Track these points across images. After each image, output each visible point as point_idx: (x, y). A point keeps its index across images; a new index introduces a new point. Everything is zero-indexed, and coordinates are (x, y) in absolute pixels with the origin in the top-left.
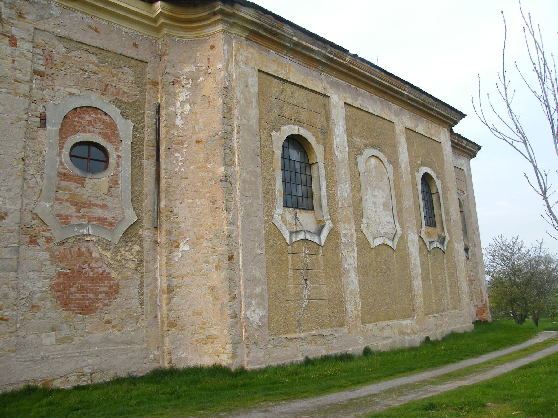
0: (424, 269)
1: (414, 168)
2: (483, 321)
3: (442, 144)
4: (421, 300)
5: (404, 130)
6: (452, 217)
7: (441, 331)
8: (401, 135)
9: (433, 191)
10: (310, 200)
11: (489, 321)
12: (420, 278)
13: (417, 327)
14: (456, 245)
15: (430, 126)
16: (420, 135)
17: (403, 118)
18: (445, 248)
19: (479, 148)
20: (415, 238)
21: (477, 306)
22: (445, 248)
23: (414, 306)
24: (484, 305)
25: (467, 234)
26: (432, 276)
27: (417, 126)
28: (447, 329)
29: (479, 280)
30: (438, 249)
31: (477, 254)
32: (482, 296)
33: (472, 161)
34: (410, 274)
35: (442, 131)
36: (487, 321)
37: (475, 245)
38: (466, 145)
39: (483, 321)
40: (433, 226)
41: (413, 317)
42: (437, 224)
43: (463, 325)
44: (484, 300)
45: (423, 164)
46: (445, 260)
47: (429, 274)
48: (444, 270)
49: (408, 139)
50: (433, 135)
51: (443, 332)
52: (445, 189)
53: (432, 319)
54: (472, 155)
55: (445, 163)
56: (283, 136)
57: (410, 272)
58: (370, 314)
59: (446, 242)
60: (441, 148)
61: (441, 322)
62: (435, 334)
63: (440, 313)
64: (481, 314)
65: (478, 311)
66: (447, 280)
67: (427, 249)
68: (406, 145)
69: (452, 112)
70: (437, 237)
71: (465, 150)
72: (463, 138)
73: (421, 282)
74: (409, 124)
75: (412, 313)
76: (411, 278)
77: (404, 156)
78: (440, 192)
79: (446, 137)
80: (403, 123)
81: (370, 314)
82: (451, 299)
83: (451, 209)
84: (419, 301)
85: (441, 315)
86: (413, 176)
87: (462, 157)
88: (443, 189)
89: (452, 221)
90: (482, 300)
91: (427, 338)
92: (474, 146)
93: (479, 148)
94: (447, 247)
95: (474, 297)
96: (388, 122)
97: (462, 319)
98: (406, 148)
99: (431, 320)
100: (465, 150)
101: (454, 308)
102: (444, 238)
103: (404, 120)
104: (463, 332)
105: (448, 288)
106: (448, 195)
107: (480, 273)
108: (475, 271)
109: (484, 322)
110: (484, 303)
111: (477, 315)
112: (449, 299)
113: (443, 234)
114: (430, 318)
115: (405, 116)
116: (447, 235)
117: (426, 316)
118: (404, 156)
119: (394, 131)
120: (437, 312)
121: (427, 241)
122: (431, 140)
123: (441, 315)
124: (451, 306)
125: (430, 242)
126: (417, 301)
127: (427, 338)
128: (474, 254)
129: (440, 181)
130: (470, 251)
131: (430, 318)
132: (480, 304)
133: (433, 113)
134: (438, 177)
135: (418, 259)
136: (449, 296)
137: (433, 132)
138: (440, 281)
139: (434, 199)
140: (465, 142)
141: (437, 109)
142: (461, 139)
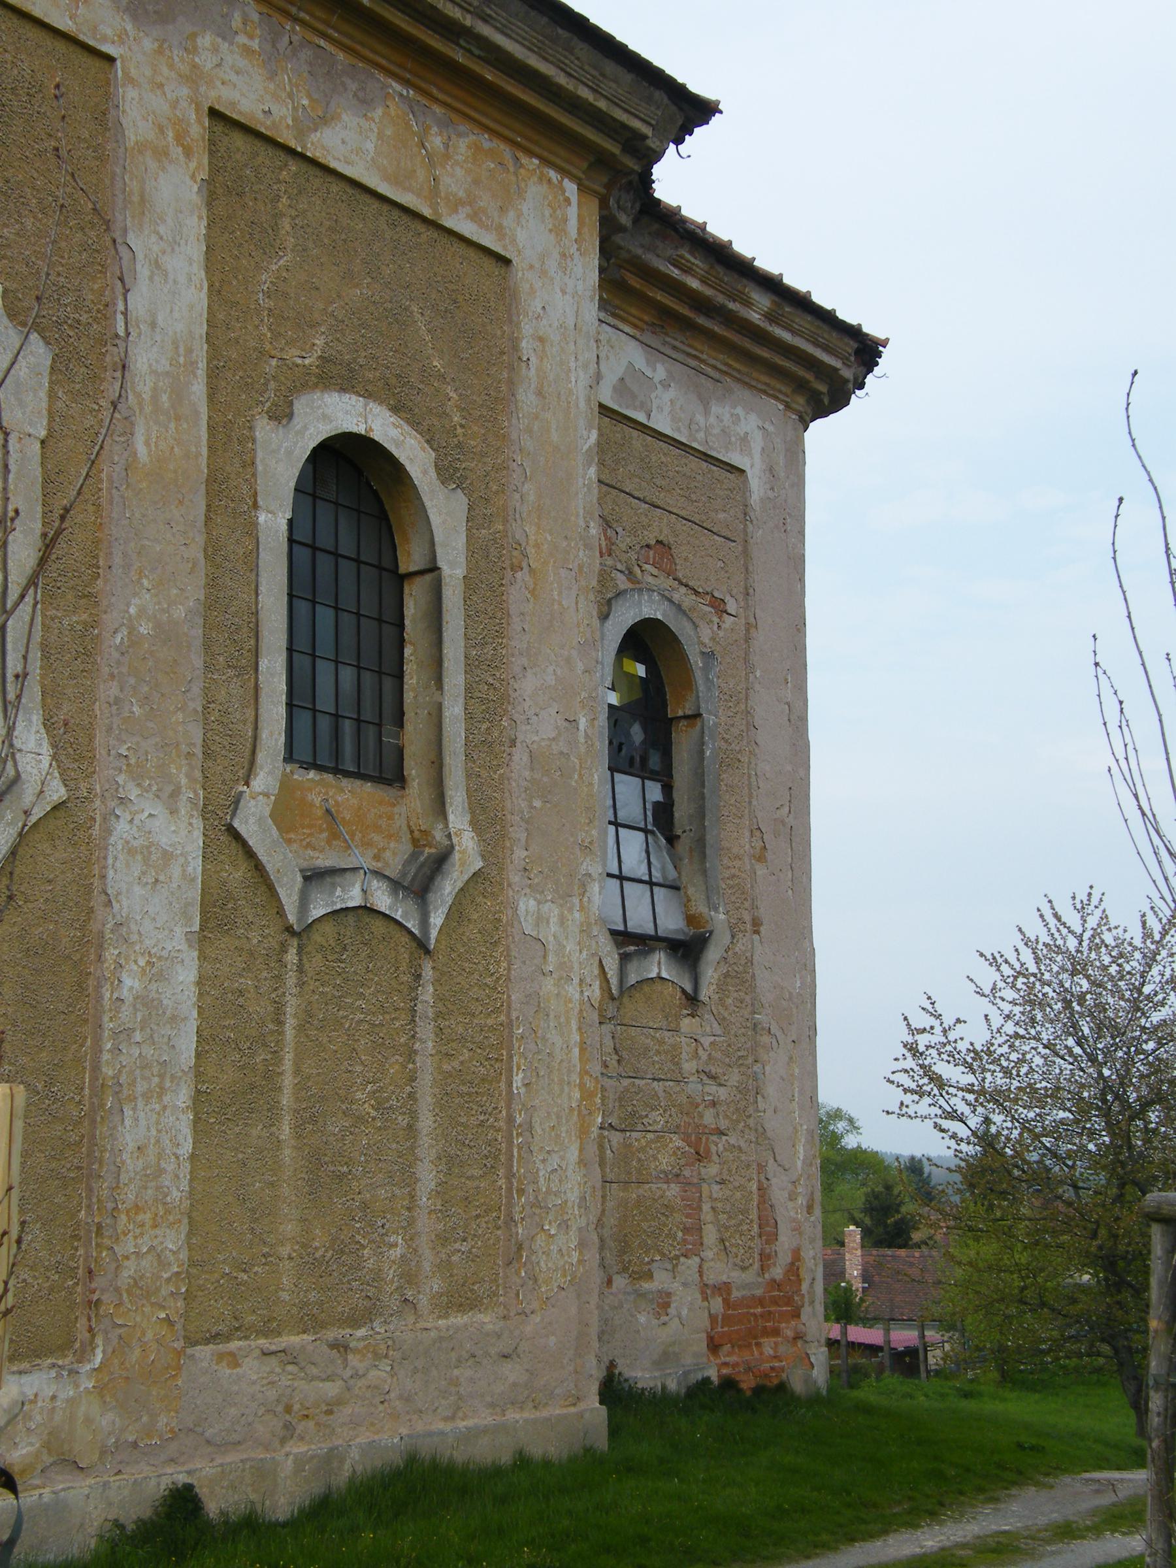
0: (233, 1041)
1: (241, 382)
2: (747, 1383)
3: (521, 271)
4: (173, 1241)
5: (198, 128)
6: (525, 735)
7: (319, 1447)
8: (161, 154)
9: (411, 559)
10: (388, 683)
11: (798, 1386)
12: (183, 1096)
13: (107, 1420)
14: (527, 905)
15: (436, 141)
16: (336, 187)
17: (206, 40)
18: (437, 920)
19: (867, 351)
20: (182, 835)
21: (723, 1289)
22: (437, 920)
23: (99, 1282)
24: (774, 1284)
25: (703, 856)
26: (299, 1087)
27: (324, 120)
28: (369, 1439)
29: (762, 1133)
30: (378, 926)
31: (764, 982)
32: (768, 1229)
33: (822, 435)
34: (96, 1068)
35: (535, 191)
36: (782, 1387)
37: (756, 924)
38: (770, 317)
39: (747, 1383)
40: (380, 779)
41: (83, 1355)
42: (414, 770)
43: (513, 1415)
44: (784, 1259)
45: (336, 375)
46: (427, 994)
47: (271, 1075)
48: (411, 1054)
49: (221, 191)
50: (455, 205)
51: (332, 1457)
52: (494, 561)
53: (251, 1368)
54: (830, 395)
55: (526, 398)
56: (714, 449)
57: (98, 1049)
58: (219, 1312)
59: (448, 887)
60: (507, 300)
61: (332, 1389)
62: (263, 1472)
63: (332, 1334)
64: (749, 1338)
65: (727, 1319)
66: (426, 1122)
67: (281, 912)
68: (195, 226)
69: (610, 67)
70: (406, 848)
71: (764, 353)
72: (744, 269)
73: (184, 1125)
74: (251, 93)
75: (82, 1324)
76: (99, 1089)
77: (167, 289)
78: (453, 568)
79: (559, 229)
80: (194, 77)
81: (219, 1312)
82: (443, 1239)
83: (527, 685)
84: (150, 1249)
85: (335, 1345)
86: (229, 442)
87: (746, 394)
88: (474, 549)
89: (520, 757)
90: (766, 1259)
91: (183, 1502)
92: (833, 337)
93: (867, 351)
94: (456, 914)
95: (710, 1235)
96: (61, 46)
97: (512, 1372)
98: (195, 250)
99: (243, 1378)
100: (764, 353)
101: (459, 1299)
102: (441, 860)
103: (206, 61)
104: (506, 1458)
105: (428, 1176)
106: (516, 597)
107: (771, 1090)
108: (734, 1078)
109: (759, 1390)
110: (777, 1272)
111: (714, 1346)
112: (424, 1244)
113: (438, 835)
114: (233, 1360)
115: (227, 34)
116: (467, 843)
117: (204, 1352)
118: (167, 289)
119: (104, 117)
120: (310, 1322)
121: (283, 863)
122: (428, 234)
123: (341, 1347)
124: (436, 1285)
125: (314, 877)
126: (128, 1246)
127: (183, 1502)
128: (740, 976)
129: (460, 502)
130: (712, 954)
131: (233, 1360)
132: (745, 1281)
133: (460, 57)
134: (447, 473)
135: (186, 975)
136: (425, 1224)
137: (454, 179)
138: (360, 1119)
139: (411, 609)
140: (763, 300)
141: (485, 30)
142: (728, 278)
